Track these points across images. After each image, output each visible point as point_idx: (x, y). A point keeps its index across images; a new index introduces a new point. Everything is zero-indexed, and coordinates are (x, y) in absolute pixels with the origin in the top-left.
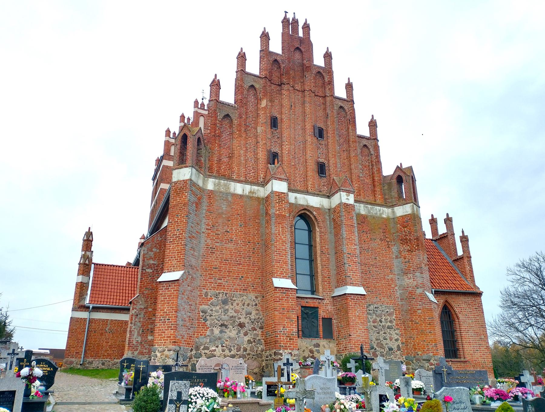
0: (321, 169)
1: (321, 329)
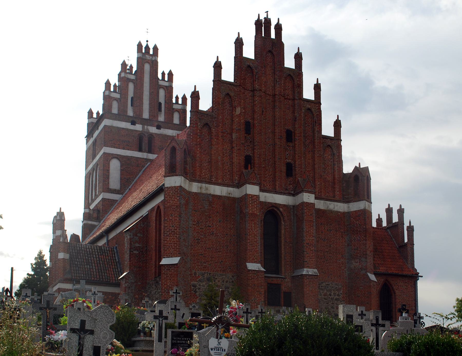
0: (290, 169)
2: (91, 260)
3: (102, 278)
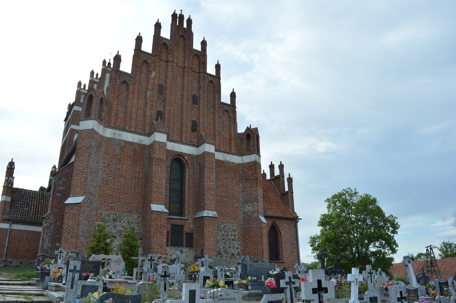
0: (195, 127)
1: (184, 240)
2: (32, 203)
3: (37, 219)
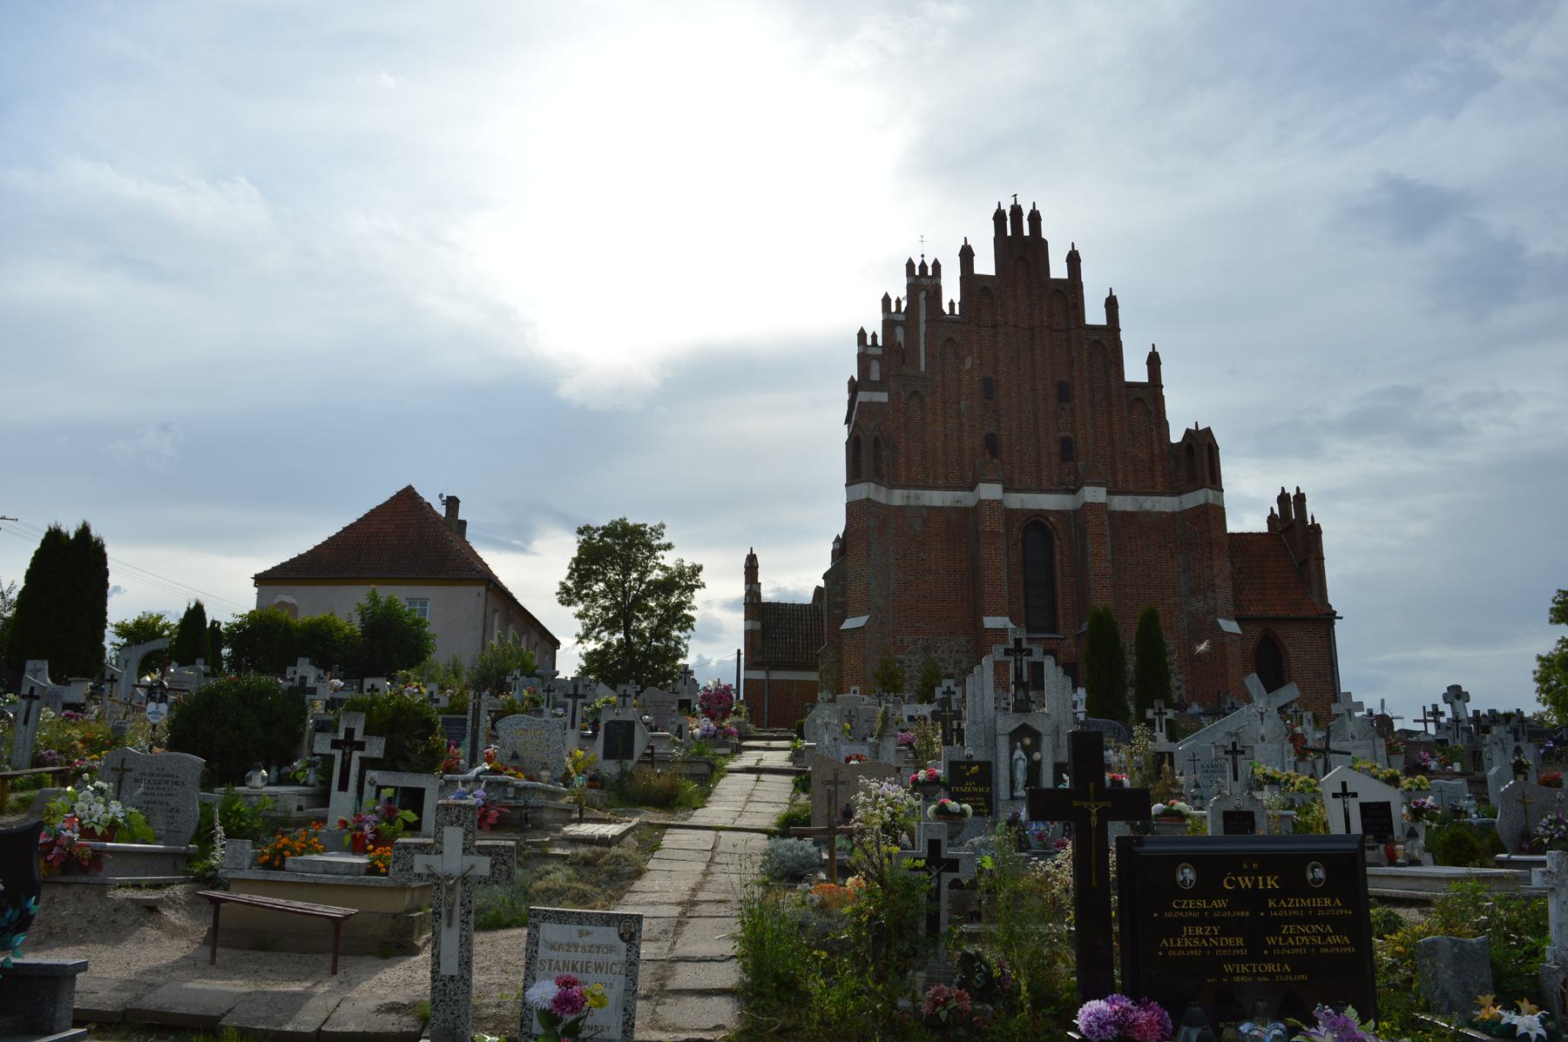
0: (1067, 450)
